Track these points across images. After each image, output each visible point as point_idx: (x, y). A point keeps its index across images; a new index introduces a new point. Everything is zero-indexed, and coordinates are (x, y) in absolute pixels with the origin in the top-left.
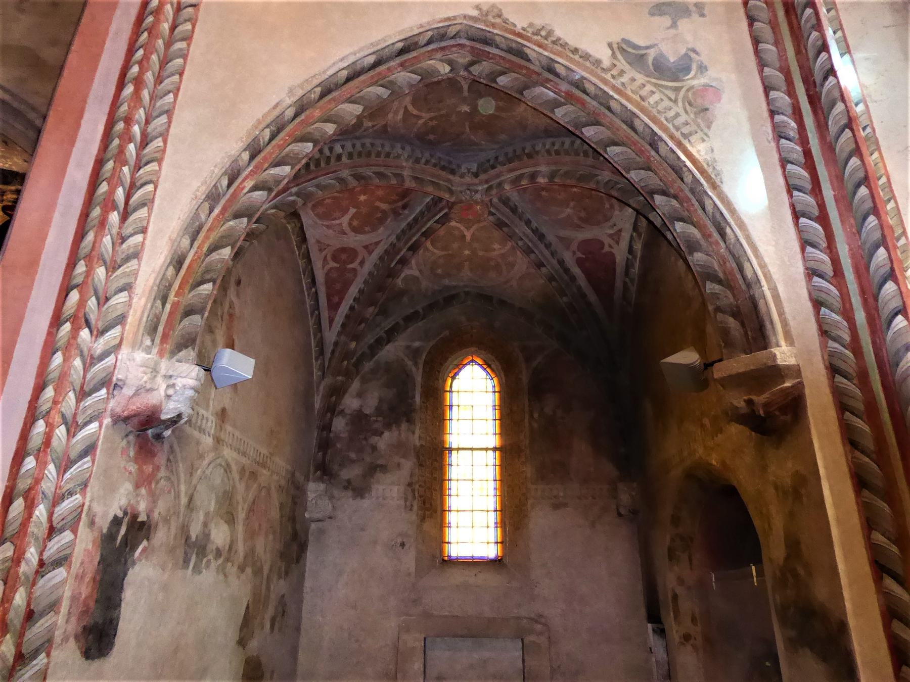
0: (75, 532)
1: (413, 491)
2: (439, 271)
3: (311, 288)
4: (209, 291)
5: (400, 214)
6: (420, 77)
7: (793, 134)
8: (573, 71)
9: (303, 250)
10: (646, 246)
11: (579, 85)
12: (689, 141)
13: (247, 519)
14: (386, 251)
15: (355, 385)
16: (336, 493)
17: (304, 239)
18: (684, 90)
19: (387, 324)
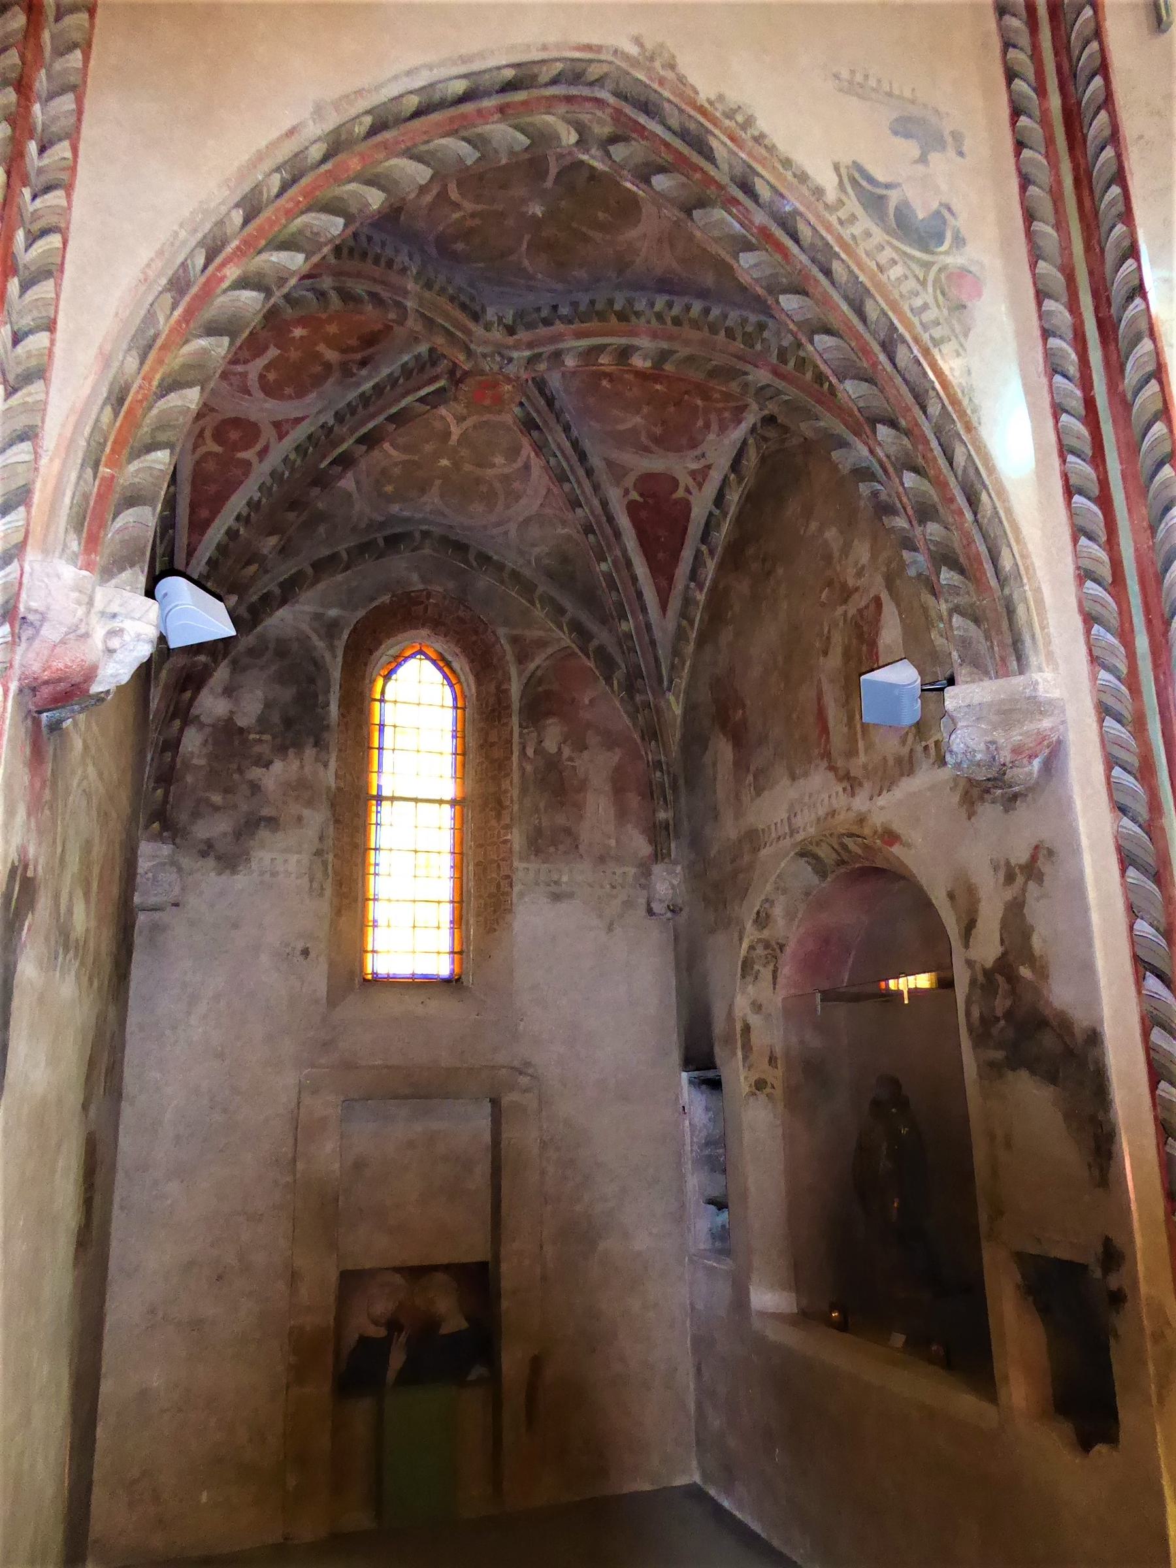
1: (325, 864)
2: (389, 488)
4: (164, 464)
5: (353, 375)
6: (528, 142)
7: (1073, 370)
8: (782, 196)
10: (751, 499)
11: (788, 224)
12: (940, 350)
14: (310, 437)
16: (186, 862)
18: (935, 269)
19: (287, 570)
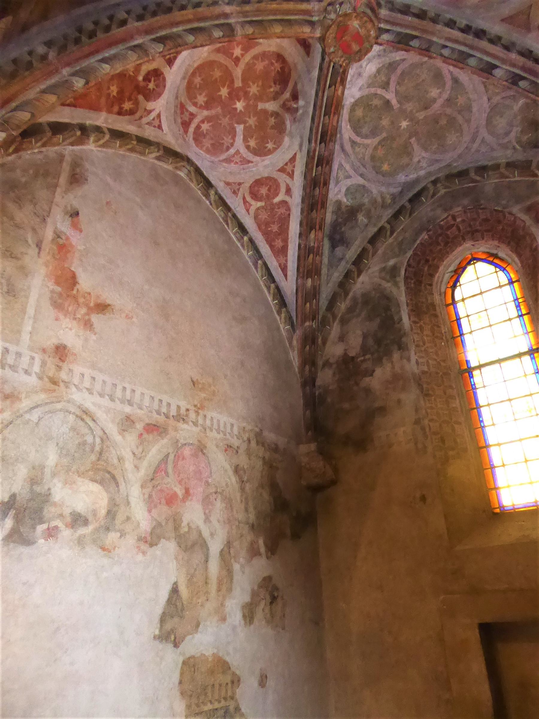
3: (243, 238)
5: (297, 110)
9: (212, 197)
15: (335, 330)
17: (208, 184)
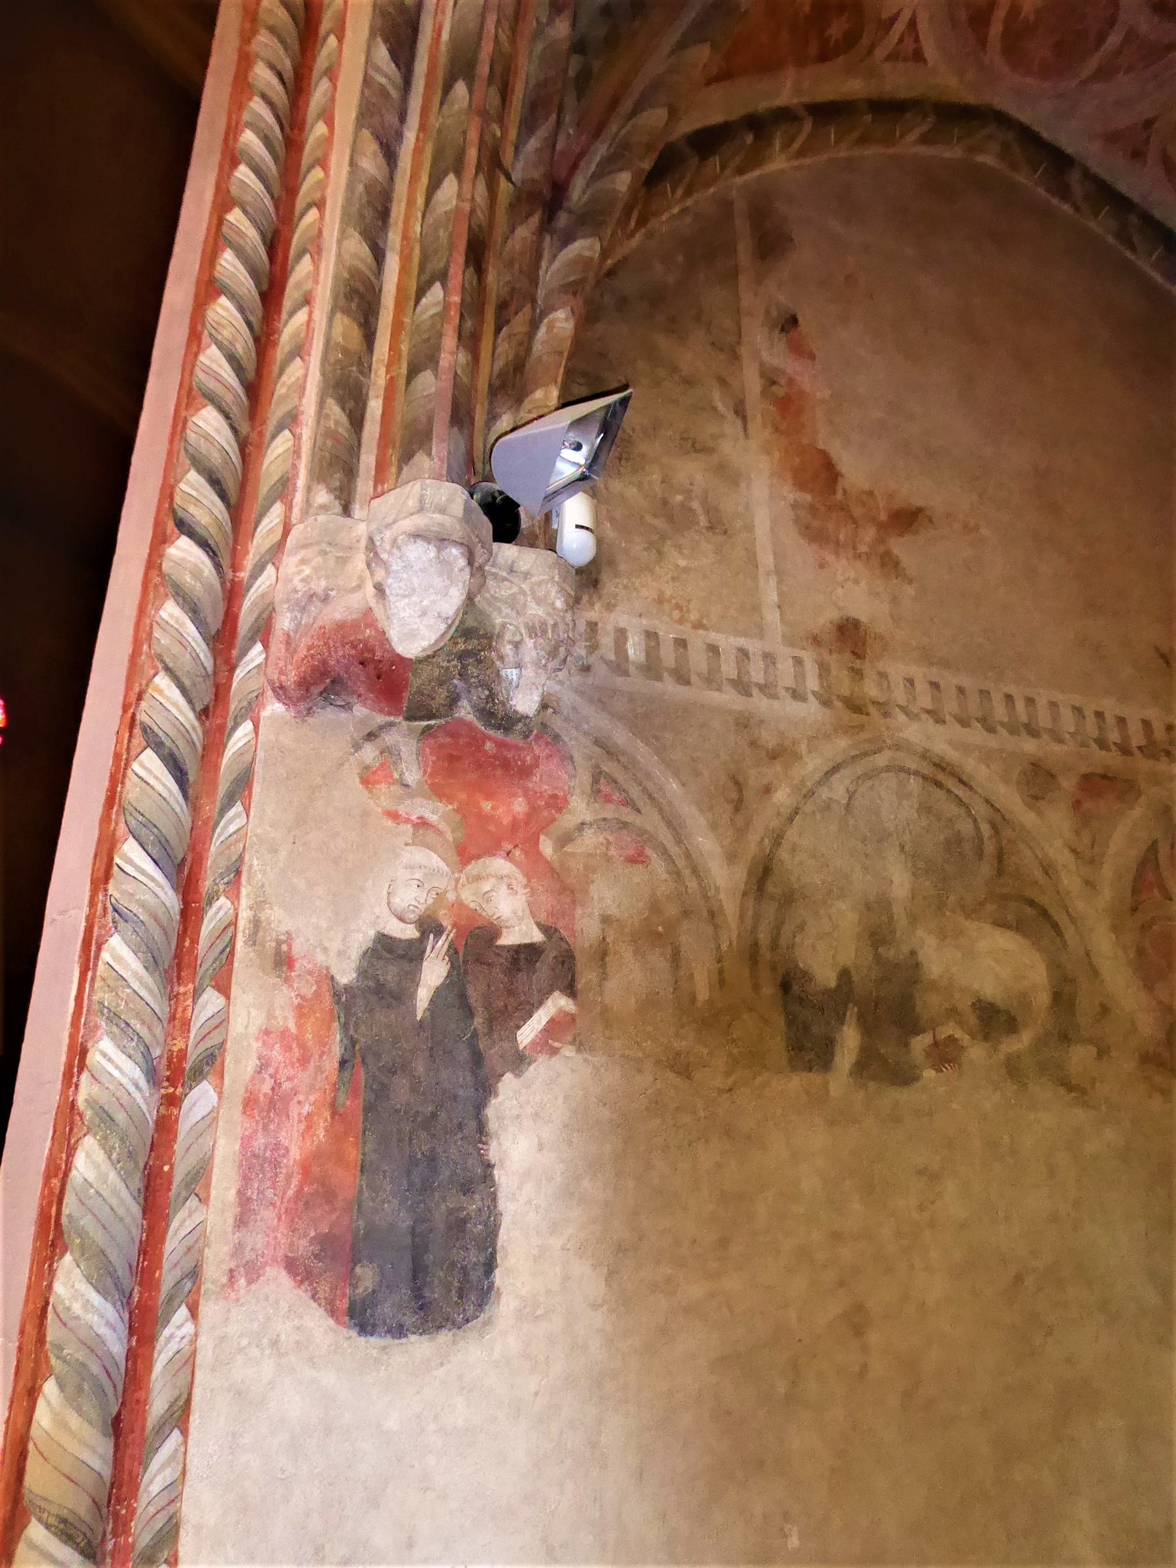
0: (224, 989)
13: (1134, 910)
